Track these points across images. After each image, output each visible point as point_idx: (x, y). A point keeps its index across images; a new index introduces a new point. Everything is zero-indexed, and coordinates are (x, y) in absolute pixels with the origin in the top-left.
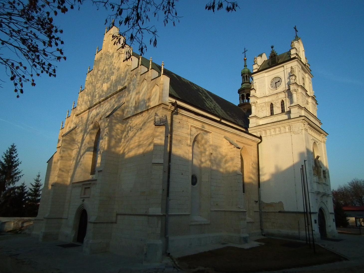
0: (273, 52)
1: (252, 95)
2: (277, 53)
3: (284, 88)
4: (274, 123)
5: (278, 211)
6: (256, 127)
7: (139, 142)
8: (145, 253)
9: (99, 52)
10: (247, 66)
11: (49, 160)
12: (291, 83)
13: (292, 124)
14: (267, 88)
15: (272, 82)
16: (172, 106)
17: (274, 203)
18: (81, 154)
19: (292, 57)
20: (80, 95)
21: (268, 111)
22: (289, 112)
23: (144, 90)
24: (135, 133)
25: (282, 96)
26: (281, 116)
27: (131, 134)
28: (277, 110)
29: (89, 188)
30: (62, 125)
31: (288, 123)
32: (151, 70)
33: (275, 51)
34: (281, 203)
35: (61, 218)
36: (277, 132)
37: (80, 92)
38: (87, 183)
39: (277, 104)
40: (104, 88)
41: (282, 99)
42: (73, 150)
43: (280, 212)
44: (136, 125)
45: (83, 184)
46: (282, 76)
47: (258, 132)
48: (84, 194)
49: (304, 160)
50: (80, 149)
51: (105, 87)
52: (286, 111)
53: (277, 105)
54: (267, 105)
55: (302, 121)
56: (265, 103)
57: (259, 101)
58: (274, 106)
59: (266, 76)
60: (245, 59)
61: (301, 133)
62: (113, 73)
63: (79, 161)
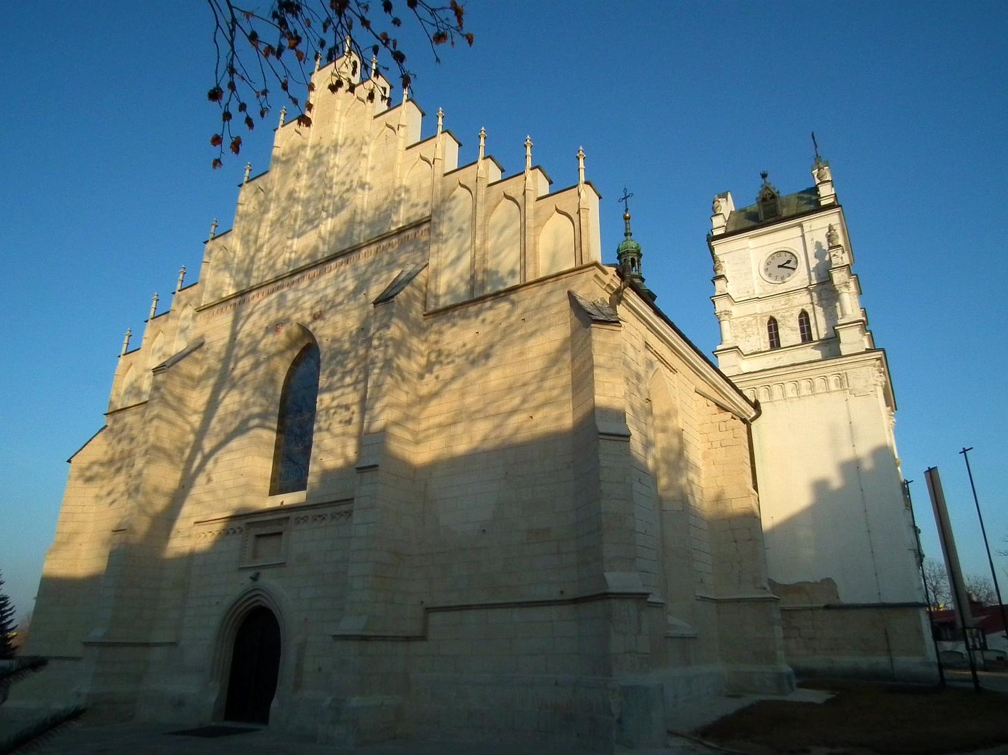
1: (720, 292)
5: (823, 605)
6: (742, 377)
8: (616, 717)
9: (286, 124)
10: (631, 234)
13: (847, 371)
14: (754, 278)
15: (768, 264)
16: (615, 274)
17: (809, 582)
19: (823, 203)
21: (764, 339)
22: (826, 341)
25: (803, 301)
28: (790, 334)
29: (280, 534)
32: (530, 171)
34: (828, 582)
35: (147, 645)
36: (804, 391)
37: (213, 239)
38: (268, 518)
39: (790, 319)
41: (804, 307)
43: (827, 607)
45: (248, 524)
46: (798, 249)
48: (255, 556)
49: (964, 448)
52: (815, 338)
53: (789, 321)
55: (874, 362)
56: (755, 315)
57: (736, 310)
58: (779, 324)
59: (751, 247)
60: (628, 215)
61: (874, 393)
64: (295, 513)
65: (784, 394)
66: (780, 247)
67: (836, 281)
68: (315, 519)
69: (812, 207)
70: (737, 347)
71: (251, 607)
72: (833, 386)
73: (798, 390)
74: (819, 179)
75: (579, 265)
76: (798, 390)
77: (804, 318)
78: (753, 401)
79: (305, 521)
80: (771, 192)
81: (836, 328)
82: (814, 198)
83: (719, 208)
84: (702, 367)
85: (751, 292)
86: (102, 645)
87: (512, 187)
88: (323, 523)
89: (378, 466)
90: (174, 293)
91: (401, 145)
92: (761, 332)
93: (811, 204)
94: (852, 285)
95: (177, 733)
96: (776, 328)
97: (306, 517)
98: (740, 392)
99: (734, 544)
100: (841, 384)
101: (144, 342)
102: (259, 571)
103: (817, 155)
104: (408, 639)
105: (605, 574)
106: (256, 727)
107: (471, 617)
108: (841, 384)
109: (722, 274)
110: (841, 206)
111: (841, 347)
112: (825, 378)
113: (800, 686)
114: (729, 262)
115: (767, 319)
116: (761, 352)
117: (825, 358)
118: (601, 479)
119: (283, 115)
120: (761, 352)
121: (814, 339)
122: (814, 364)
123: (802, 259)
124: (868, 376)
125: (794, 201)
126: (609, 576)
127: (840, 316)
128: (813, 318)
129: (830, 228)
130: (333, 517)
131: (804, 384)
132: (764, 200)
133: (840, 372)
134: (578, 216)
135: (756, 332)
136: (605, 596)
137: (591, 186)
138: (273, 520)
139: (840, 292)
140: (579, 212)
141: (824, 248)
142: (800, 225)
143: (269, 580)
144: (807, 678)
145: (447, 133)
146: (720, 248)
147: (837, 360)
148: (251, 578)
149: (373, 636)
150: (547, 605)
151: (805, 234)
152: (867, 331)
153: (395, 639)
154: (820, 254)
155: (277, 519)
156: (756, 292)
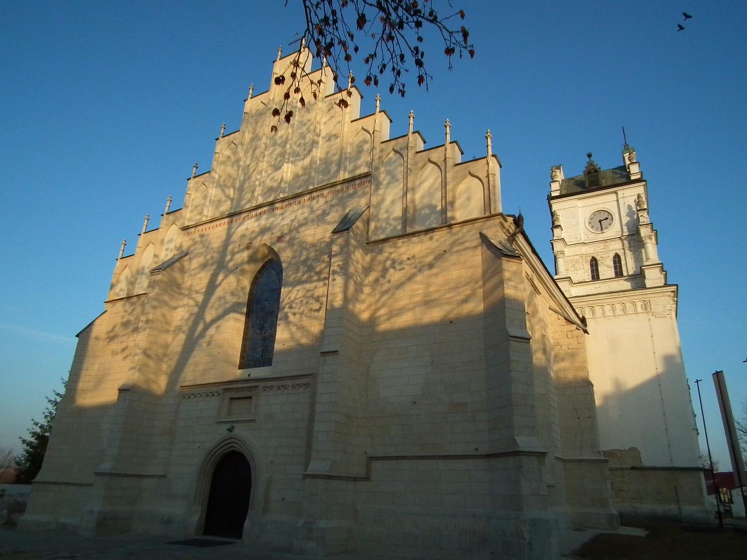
0: (591, 164)
1: (558, 237)
2: (600, 168)
3: (619, 231)
4: (612, 294)
5: (629, 467)
7: (427, 294)
11: (84, 330)
12: (642, 224)
13: (650, 299)
16: (513, 222)
18: (208, 317)
19: (633, 178)
20: (192, 183)
21: (588, 272)
23: (426, 186)
24: (408, 275)
25: (616, 247)
26: (617, 283)
27: (395, 276)
28: (606, 270)
29: (250, 398)
30: (122, 248)
31: (640, 297)
33: (595, 163)
34: (634, 450)
35: (141, 476)
36: (618, 312)
37: (194, 177)
38: (240, 386)
40: (287, 172)
42: (176, 308)
43: (633, 468)
44: (413, 257)
45: (224, 389)
46: (613, 210)
47: (616, 304)
48: (229, 413)
50: (203, 307)
51: (288, 171)
52: (625, 274)
54: (584, 260)
55: (670, 293)
56: (581, 255)
57: (567, 251)
58: (599, 262)
62: (317, 143)
63: (202, 335)
64: (262, 383)
65: (604, 313)
66: (600, 207)
67: (642, 235)
68: (279, 388)
69: (624, 180)
70: (570, 278)
71: (227, 451)
72: (639, 309)
73: (614, 311)
74: (630, 160)
75: (487, 214)
76: (614, 311)
77: (617, 259)
78: (581, 317)
79: (286, 388)
80: (595, 167)
81: (643, 268)
82: (625, 173)
83: (556, 177)
84: (554, 291)
85: (579, 239)
86: (111, 475)
87: (436, 155)
88: (286, 391)
89: (337, 351)
90: (162, 215)
91: (347, 119)
92: (585, 267)
93: (623, 178)
94: (653, 238)
95: (170, 543)
96: (597, 265)
97: (271, 386)
98: (574, 310)
99: (578, 420)
100: (646, 308)
101: (138, 250)
102: (234, 424)
103: (626, 143)
104: (355, 479)
105: (515, 437)
106: (232, 540)
107: (405, 464)
108: (646, 308)
109: (559, 224)
110: (645, 181)
111: (646, 281)
112: (634, 304)
113: (622, 524)
114: (562, 216)
115: (590, 258)
116: (586, 282)
117: (633, 289)
118: (512, 369)
119: (251, 90)
120: (586, 282)
121: (624, 275)
122: (626, 293)
123: (616, 217)
124: (664, 302)
125: (610, 175)
126: (518, 439)
127: (644, 260)
128: (624, 260)
129: (639, 196)
130: (294, 387)
131: (618, 306)
132: (589, 173)
133: (645, 300)
134: (487, 179)
135: (582, 268)
136: (517, 453)
137: (496, 158)
138: (245, 387)
139: (645, 242)
140: (488, 176)
141: (633, 209)
142: (616, 193)
143: (241, 432)
144: (626, 519)
145: (383, 113)
146: (557, 206)
147: (644, 291)
148: (228, 429)
149: (335, 476)
150: (432, 459)
151: (619, 200)
152: (663, 271)
153: (347, 479)
154: (630, 213)
155: (248, 387)
156: (582, 239)
